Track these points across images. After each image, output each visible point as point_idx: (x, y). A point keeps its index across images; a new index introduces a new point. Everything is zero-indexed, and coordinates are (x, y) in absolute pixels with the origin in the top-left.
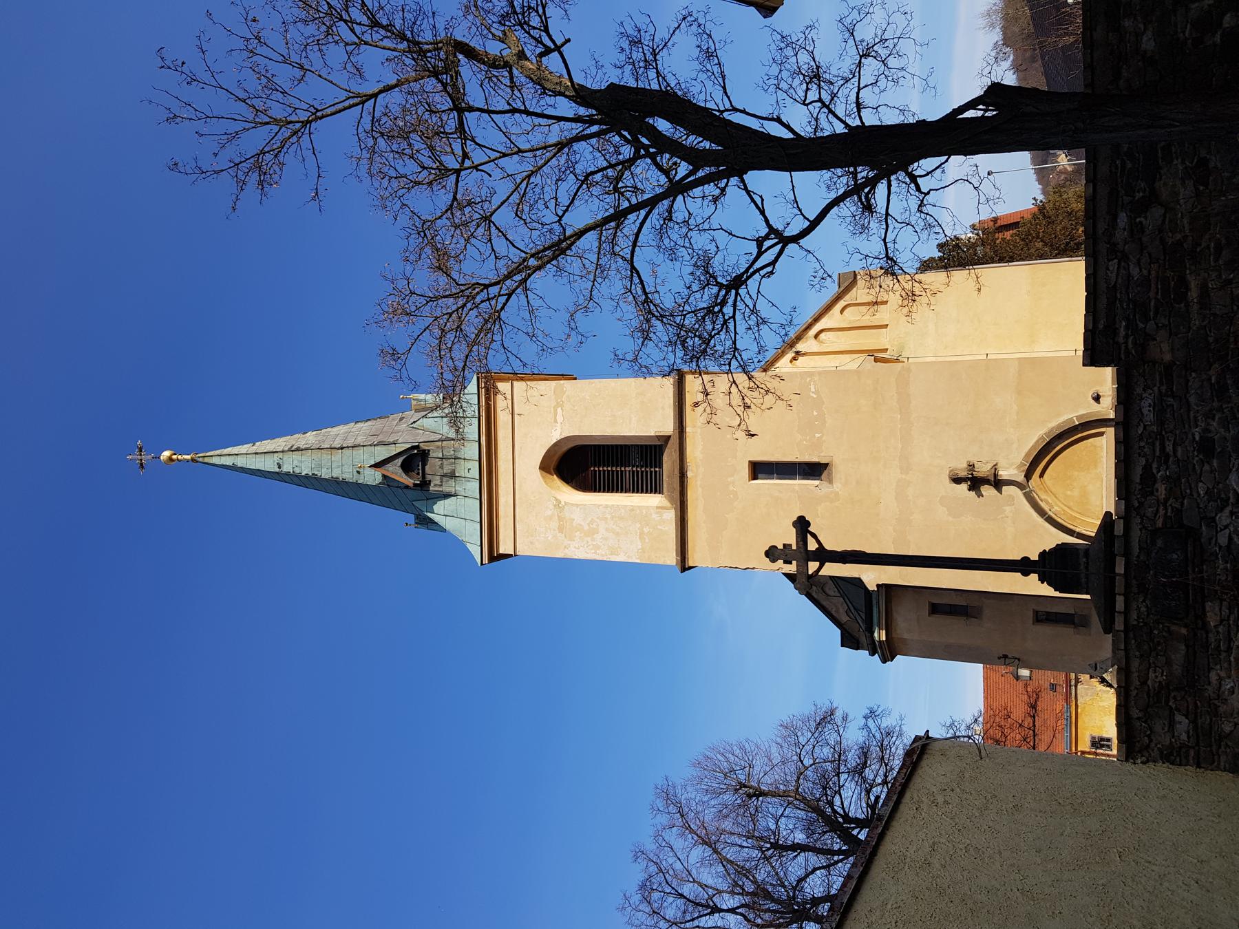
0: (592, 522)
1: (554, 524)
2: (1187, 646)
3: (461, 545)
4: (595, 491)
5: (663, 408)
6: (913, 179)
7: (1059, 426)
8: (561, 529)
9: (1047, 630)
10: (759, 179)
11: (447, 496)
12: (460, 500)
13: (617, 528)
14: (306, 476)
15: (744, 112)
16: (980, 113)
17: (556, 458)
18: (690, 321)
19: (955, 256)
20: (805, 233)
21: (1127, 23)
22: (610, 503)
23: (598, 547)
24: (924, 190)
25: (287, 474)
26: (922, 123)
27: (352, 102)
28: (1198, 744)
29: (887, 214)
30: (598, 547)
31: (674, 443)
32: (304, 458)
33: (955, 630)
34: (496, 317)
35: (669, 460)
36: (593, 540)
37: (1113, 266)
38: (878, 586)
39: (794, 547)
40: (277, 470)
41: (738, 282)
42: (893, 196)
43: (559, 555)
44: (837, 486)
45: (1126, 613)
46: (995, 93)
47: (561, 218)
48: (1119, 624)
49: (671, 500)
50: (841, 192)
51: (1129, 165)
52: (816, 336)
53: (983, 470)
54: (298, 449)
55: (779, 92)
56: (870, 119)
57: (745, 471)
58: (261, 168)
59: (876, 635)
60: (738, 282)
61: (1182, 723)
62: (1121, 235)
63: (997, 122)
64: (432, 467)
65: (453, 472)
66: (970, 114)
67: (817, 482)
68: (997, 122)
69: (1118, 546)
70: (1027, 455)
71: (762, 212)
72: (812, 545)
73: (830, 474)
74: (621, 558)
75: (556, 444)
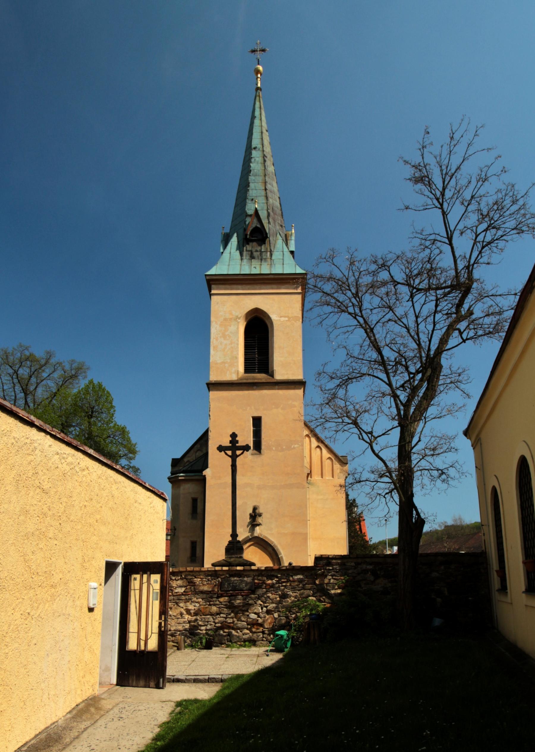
0: (230, 337)
1: (228, 316)
2: (210, 591)
3: (214, 263)
6: (391, 492)
7: (278, 549)
8: (225, 319)
9: (188, 546)
10: (397, 432)
11: (241, 255)
12: (239, 261)
15: (424, 427)
16: (414, 515)
17: (262, 316)
19: (350, 505)
20: (373, 451)
21: (442, 567)
22: (239, 346)
23: (217, 339)
24: (386, 496)
25: (251, 154)
26: (412, 495)
27: (449, 233)
28: (174, 596)
29: (378, 482)
30: (217, 339)
32: (260, 165)
33: (186, 508)
34: (342, 309)
35: (261, 377)
36: (220, 337)
37: (353, 564)
38: (205, 476)
39: (237, 445)
40: (253, 146)
41: (355, 423)
42: (385, 485)
43: (212, 319)
45: (222, 570)
46: (421, 522)
47: (388, 346)
48: (217, 568)
49: (241, 379)
50: (389, 465)
51: (390, 569)
53: (259, 520)
54: (265, 161)
55: (430, 437)
56: (417, 474)
57: (256, 415)
58: (422, 178)
59: (182, 474)
60: (355, 423)
61: (182, 590)
62: (364, 567)
63: (410, 520)
66: (414, 512)
68: (410, 520)
69: (247, 568)
70: (266, 537)
71: (383, 434)
72: (238, 452)
73: (256, 454)
74: (212, 352)
75: (269, 318)
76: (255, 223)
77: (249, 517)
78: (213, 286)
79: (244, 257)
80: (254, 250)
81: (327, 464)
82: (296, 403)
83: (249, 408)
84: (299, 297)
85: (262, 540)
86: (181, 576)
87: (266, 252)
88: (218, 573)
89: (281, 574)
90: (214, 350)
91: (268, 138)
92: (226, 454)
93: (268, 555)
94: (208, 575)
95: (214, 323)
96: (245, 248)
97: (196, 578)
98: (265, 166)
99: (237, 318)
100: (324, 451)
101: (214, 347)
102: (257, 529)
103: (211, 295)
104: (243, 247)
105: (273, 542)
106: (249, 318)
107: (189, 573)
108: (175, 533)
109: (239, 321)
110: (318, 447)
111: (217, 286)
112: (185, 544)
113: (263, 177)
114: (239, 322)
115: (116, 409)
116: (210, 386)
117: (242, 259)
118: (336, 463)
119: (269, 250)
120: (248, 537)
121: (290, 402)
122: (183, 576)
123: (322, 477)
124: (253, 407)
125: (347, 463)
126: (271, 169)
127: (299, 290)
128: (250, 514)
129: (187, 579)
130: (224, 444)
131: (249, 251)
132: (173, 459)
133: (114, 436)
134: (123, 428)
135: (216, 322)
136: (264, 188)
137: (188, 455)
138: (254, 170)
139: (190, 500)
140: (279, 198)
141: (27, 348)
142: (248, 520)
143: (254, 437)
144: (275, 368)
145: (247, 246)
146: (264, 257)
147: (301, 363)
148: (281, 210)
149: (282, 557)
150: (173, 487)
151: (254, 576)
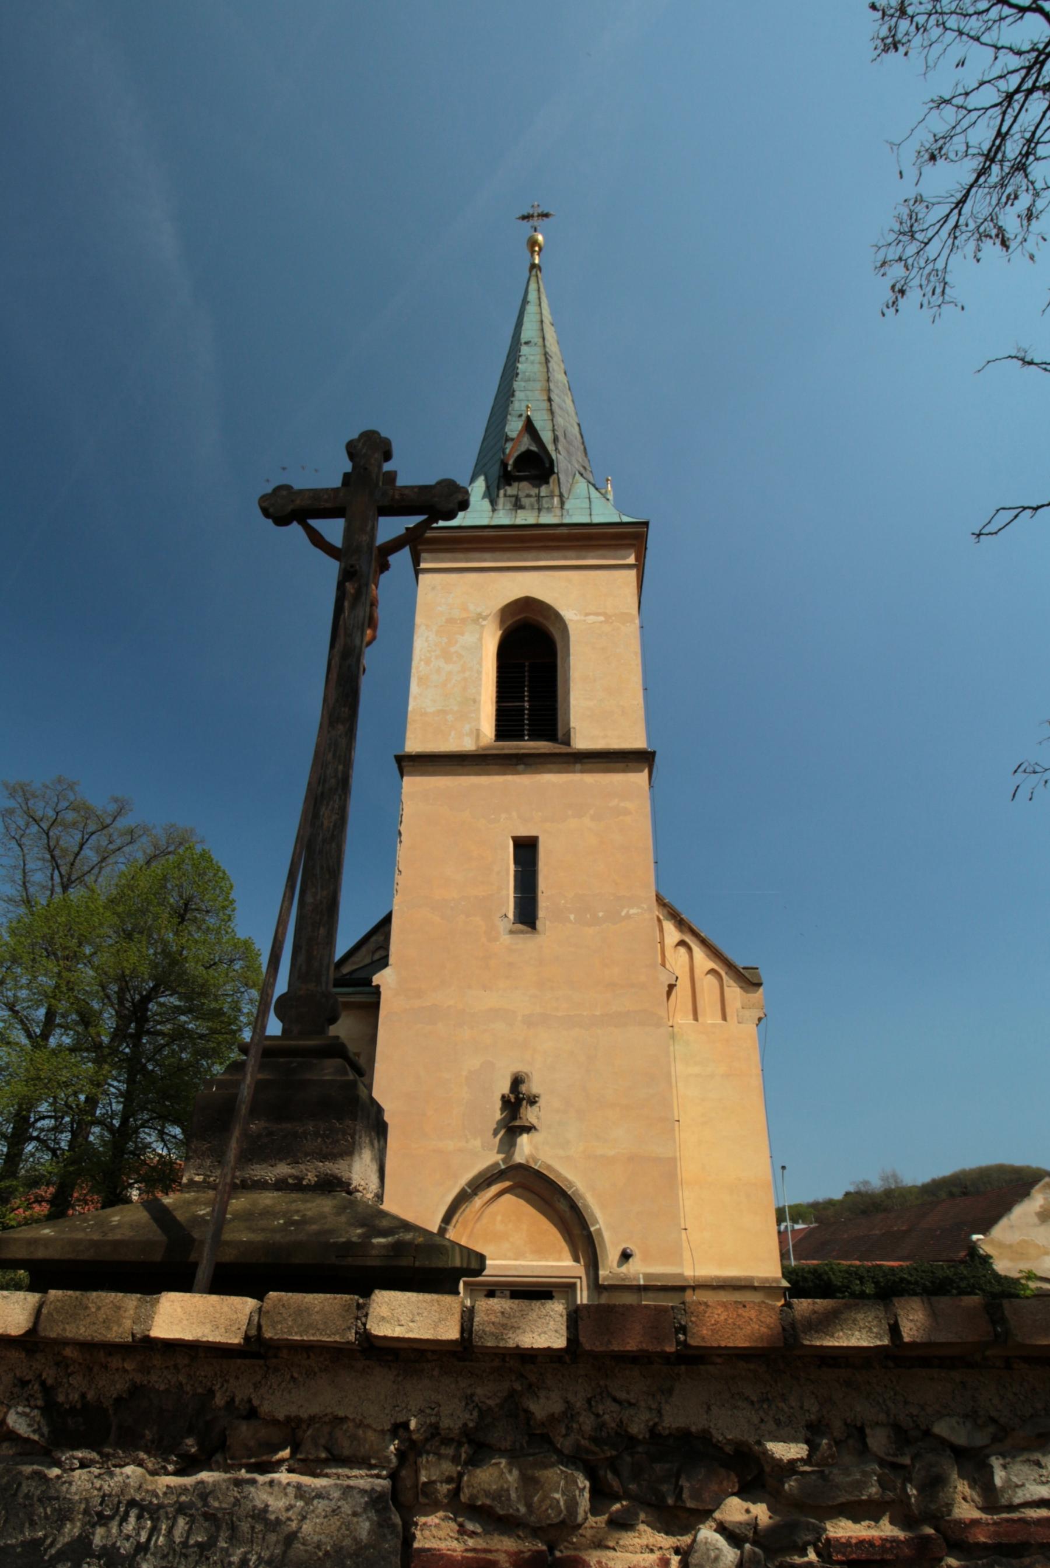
4: (497, 720)
7: (587, 1206)
8: (451, 621)
17: (541, 619)
18: (425, 1314)
22: (484, 677)
23: (428, 662)
30: (428, 662)
31: (564, 749)
38: (378, 987)
40: (523, 341)
43: (419, 619)
44: (506, 939)
53: (530, 1115)
57: (524, 831)
64: (523, 489)
65: (522, 507)
67: (511, 916)
69: (312, 1314)
70: (549, 1167)
73: (522, 932)
74: (414, 688)
76: (526, 444)
77: (498, 1104)
78: (424, 555)
79: (500, 506)
80: (521, 494)
81: (708, 986)
82: (628, 805)
83: (503, 816)
84: (633, 573)
85: (539, 1175)
87: (552, 496)
89: (811, 1435)
90: (418, 685)
91: (554, 335)
92: (317, 540)
93: (555, 1225)
95: (423, 627)
96: (502, 492)
98: (548, 368)
99: (480, 617)
100: (699, 953)
101: (420, 679)
102: (524, 1140)
103: (417, 572)
104: (499, 489)
105: (571, 1185)
106: (509, 623)
109: (484, 623)
110: (682, 943)
111: (433, 555)
114: (483, 626)
116: (404, 764)
117: (494, 510)
118: (732, 983)
119: (557, 493)
120: (497, 1164)
121: (614, 802)
123: (696, 1019)
124: (514, 814)
125: (759, 985)
126: (559, 375)
127: (631, 560)
128: (503, 1097)
130: (304, 480)
131: (510, 496)
134: (245, 942)
135: (427, 626)
136: (546, 398)
140: (579, 425)
141: (71, 787)
142: (498, 1116)
143: (517, 888)
144: (572, 725)
145: (507, 488)
147: (641, 713)
148: (583, 443)
149: (599, 1231)
151: (411, 1452)
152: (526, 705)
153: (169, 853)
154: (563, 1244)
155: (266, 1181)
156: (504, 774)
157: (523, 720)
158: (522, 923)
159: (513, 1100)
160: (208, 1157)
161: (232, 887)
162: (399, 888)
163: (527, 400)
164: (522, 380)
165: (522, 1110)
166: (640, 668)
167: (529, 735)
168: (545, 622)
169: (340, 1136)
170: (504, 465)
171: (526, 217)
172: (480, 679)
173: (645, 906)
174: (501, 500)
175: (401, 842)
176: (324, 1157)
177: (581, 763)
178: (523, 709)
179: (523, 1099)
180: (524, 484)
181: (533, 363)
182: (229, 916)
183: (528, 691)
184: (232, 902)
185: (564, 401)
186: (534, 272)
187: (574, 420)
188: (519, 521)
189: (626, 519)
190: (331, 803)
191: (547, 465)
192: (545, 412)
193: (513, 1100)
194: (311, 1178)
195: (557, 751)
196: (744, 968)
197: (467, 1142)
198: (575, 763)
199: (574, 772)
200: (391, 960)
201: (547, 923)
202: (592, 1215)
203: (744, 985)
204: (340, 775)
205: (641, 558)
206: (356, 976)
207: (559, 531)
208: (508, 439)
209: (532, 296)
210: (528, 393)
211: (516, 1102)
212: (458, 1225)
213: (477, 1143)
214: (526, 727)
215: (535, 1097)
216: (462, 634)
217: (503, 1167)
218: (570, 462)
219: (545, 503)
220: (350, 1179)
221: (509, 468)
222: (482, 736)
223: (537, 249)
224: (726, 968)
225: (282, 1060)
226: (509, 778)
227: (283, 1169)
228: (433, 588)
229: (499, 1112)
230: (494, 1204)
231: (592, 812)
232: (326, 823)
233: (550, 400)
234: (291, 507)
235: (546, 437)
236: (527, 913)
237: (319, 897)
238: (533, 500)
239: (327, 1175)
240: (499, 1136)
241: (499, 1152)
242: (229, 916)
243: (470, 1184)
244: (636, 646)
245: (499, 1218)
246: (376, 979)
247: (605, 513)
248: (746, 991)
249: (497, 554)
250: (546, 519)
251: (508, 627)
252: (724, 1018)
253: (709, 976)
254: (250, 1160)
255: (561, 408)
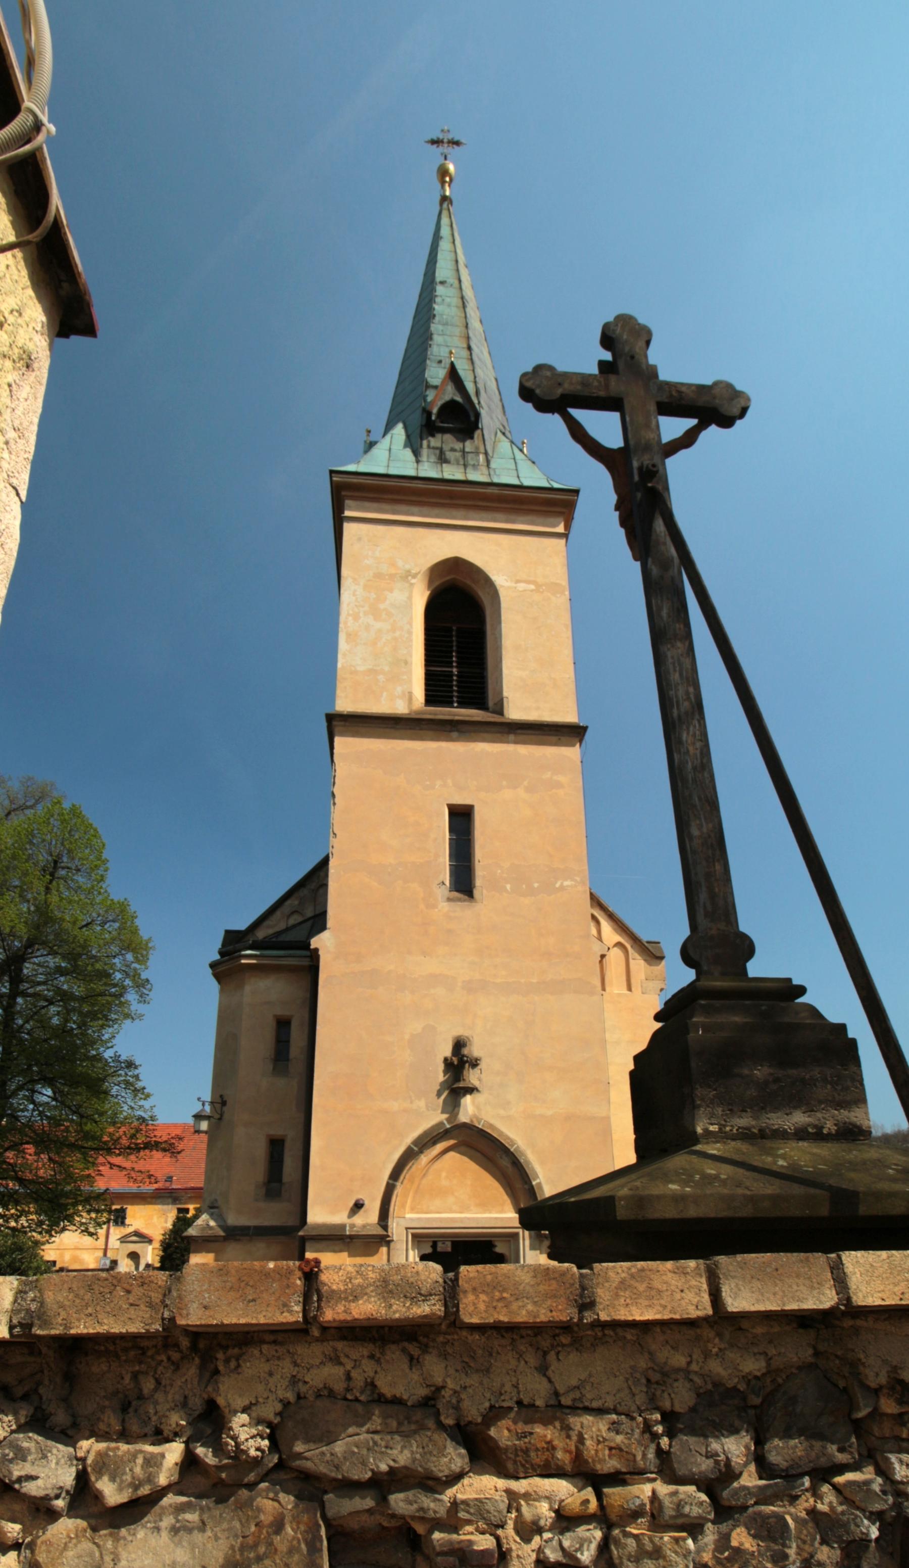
5: (538, 708)
7: (528, 1162)
8: (378, 576)
9: (261, 1151)
13: (381, 647)
14: (431, 309)
17: (468, 582)
22: (414, 637)
23: (356, 617)
25: (434, 290)
30: (356, 617)
33: (257, 1045)
38: (317, 950)
44: (444, 906)
49: (417, 712)
52: (593, 917)
53: (472, 1077)
59: (249, 952)
64: (448, 441)
67: (447, 883)
70: (491, 1126)
73: (459, 900)
74: (343, 645)
76: (450, 393)
77: (441, 1067)
78: (348, 502)
79: (424, 458)
80: (446, 448)
81: (615, 955)
82: (561, 778)
83: (439, 783)
86: (210, 1422)
87: (477, 453)
88: (876, 1360)
90: (347, 642)
91: (468, 278)
92: (578, 433)
93: (498, 1180)
94: (718, 1408)
95: (350, 580)
96: (425, 443)
97: (484, 1455)
100: (606, 927)
101: (349, 635)
104: (422, 439)
105: (513, 1143)
106: (437, 583)
107: (361, 1366)
108: (222, 1115)
109: (413, 581)
111: (358, 503)
112: (250, 1144)
113: (464, 329)
114: (412, 584)
115: (94, 826)
116: (334, 723)
117: (418, 462)
120: (441, 1124)
121: (548, 775)
122: (246, 1434)
124: (449, 782)
125: (662, 958)
126: (475, 324)
127: (560, 529)
128: (446, 1059)
129: (310, 1487)
131: (434, 448)
132: (228, 932)
133: (104, 923)
135: (355, 580)
136: (465, 346)
137: (267, 923)
138: (442, 315)
139: (271, 1025)
140: (496, 380)
142: (441, 1078)
144: (505, 694)
145: (430, 438)
146: (471, 462)
147: (572, 686)
148: (501, 400)
149: (539, 1184)
150: (222, 991)
152: (455, 671)
153: (28, 807)
154: (506, 1197)
155: (785, 1130)
156: (437, 739)
157: (452, 686)
158: (458, 891)
159: (456, 1063)
160: (718, 1106)
161: (104, 845)
162: (334, 851)
163: (445, 345)
164: (439, 323)
165: (465, 1073)
166: (570, 642)
167: (458, 702)
168: (473, 586)
169: (849, 1083)
170: (429, 414)
171: (436, 142)
172: (411, 641)
173: (578, 879)
174: (425, 452)
175: (334, 804)
176: (841, 1105)
177: (515, 734)
178: (451, 674)
179: (467, 1061)
180: (448, 437)
181: (449, 305)
182: (102, 876)
183: (456, 657)
184: (105, 862)
185: (481, 351)
186: (445, 205)
187: (491, 374)
188: (447, 476)
189: (556, 485)
190: (691, 728)
191: (473, 419)
192: (465, 361)
193: (456, 1063)
194: (829, 1127)
195: (492, 720)
196: (648, 942)
197: (411, 1102)
198: (509, 733)
199: (508, 742)
200: (328, 925)
201: (485, 892)
202: (533, 1170)
203: (648, 958)
204: (692, 696)
205: (568, 527)
206: (282, 938)
207: (490, 490)
208: (428, 386)
209: (445, 231)
210: (448, 339)
211: (459, 1065)
212: (405, 1182)
213: (421, 1104)
214: (455, 694)
215: (477, 1060)
216: (391, 591)
217: (448, 1126)
218: (492, 418)
219: (470, 459)
220: (870, 1127)
221: (433, 418)
222: (414, 699)
223: (447, 179)
224: (632, 942)
225: (747, 1002)
226: (444, 744)
227: (799, 1118)
228: (360, 539)
229: (442, 1074)
230: (439, 1161)
231: (526, 783)
232: (691, 748)
233: (469, 348)
234: (559, 391)
235: (470, 387)
236: (463, 881)
237: (705, 830)
238: (458, 454)
239: (845, 1123)
240: (443, 1097)
241: (442, 1112)
242: (102, 876)
243: (415, 1142)
244: (566, 618)
245: (444, 1174)
246: (315, 942)
247: (532, 477)
248: (650, 964)
249: (425, 509)
250: (474, 476)
251: (436, 588)
252: (629, 988)
253: (615, 948)
254: (763, 1108)
255: (480, 359)
